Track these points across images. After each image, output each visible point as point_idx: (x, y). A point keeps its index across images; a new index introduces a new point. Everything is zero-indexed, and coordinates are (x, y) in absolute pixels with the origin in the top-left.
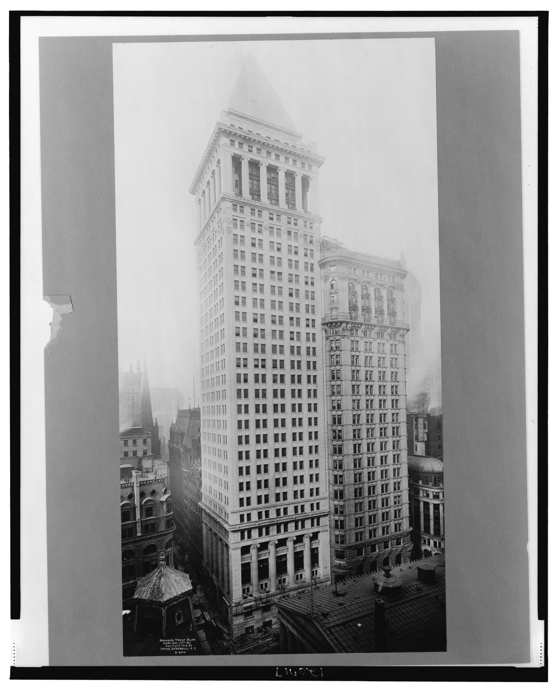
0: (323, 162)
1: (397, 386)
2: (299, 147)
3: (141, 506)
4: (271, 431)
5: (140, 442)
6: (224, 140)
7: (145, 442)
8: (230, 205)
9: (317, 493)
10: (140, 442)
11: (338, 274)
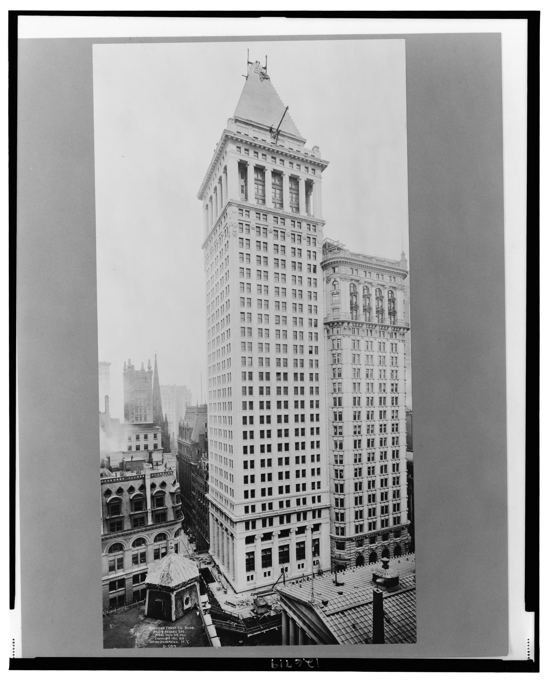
0: (326, 166)
1: (397, 425)
2: (303, 152)
3: (152, 497)
4: (274, 441)
5: (151, 436)
6: (231, 147)
7: (155, 436)
8: (236, 209)
9: (319, 501)
10: (151, 436)
11: (340, 275)
